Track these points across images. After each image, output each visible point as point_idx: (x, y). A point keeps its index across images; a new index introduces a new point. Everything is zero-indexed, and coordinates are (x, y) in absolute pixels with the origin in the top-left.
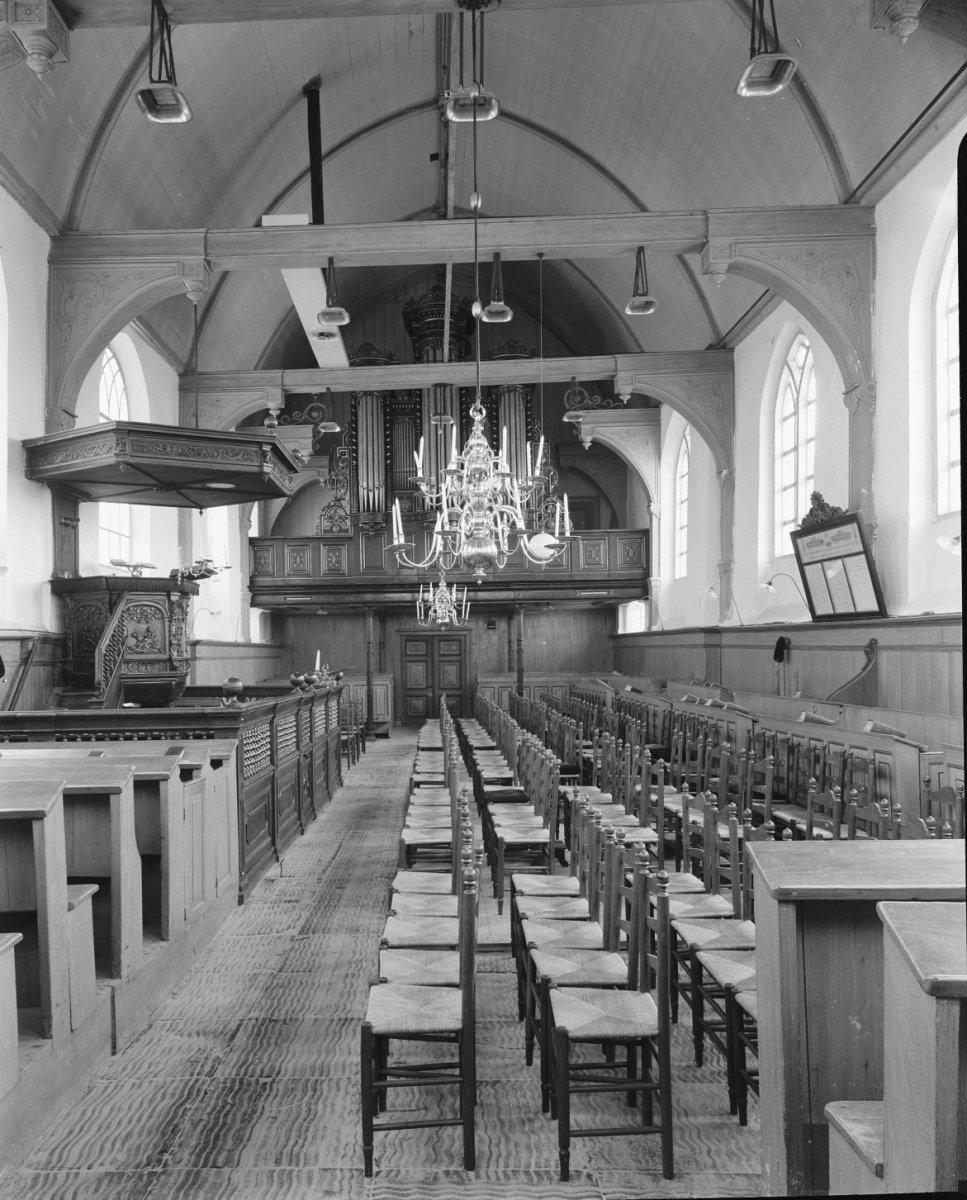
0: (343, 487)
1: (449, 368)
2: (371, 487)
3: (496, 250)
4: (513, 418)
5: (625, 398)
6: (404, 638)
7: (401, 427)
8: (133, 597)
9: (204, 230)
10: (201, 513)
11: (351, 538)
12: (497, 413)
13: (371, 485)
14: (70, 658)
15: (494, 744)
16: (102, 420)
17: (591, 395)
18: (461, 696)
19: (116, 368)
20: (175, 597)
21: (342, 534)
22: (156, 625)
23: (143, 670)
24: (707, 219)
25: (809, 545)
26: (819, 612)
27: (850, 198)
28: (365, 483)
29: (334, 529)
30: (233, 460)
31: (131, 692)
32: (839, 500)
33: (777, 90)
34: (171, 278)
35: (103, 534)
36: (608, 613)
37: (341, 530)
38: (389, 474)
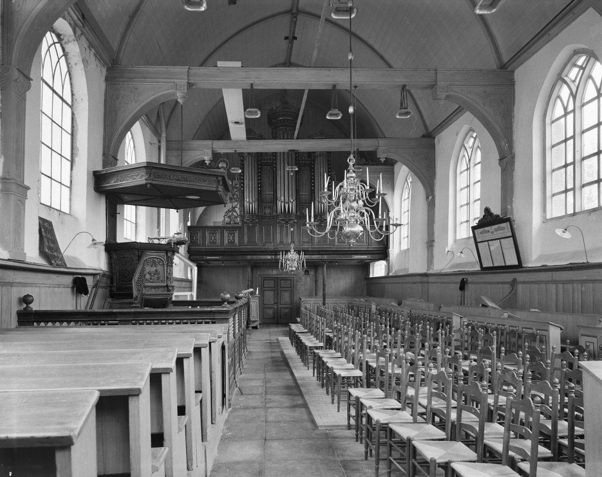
0: (236, 201)
1: (297, 142)
2: (251, 202)
3: (334, 83)
4: (322, 168)
5: (383, 160)
6: (263, 279)
8: (150, 253)
12: (314, 166)
13: (251, 200)
14: (115, 284)
15: (307, 330)
16: (126, 164)
18: (291, 308)
19: (61, 53)
20: (169, 254)
21: (236, 225)
22: (159, 268)
23: (153, 291)
24: (436, 73)
25: (481, 233)
26: (484, 266)
27: (503, 67)
28: (248, 200)
30: (203, 184)
31: (148, 303)
32: (496, 211)
33: (493, 11)
34: (171, 91)
36: (365, 267)
37: (235, 223)
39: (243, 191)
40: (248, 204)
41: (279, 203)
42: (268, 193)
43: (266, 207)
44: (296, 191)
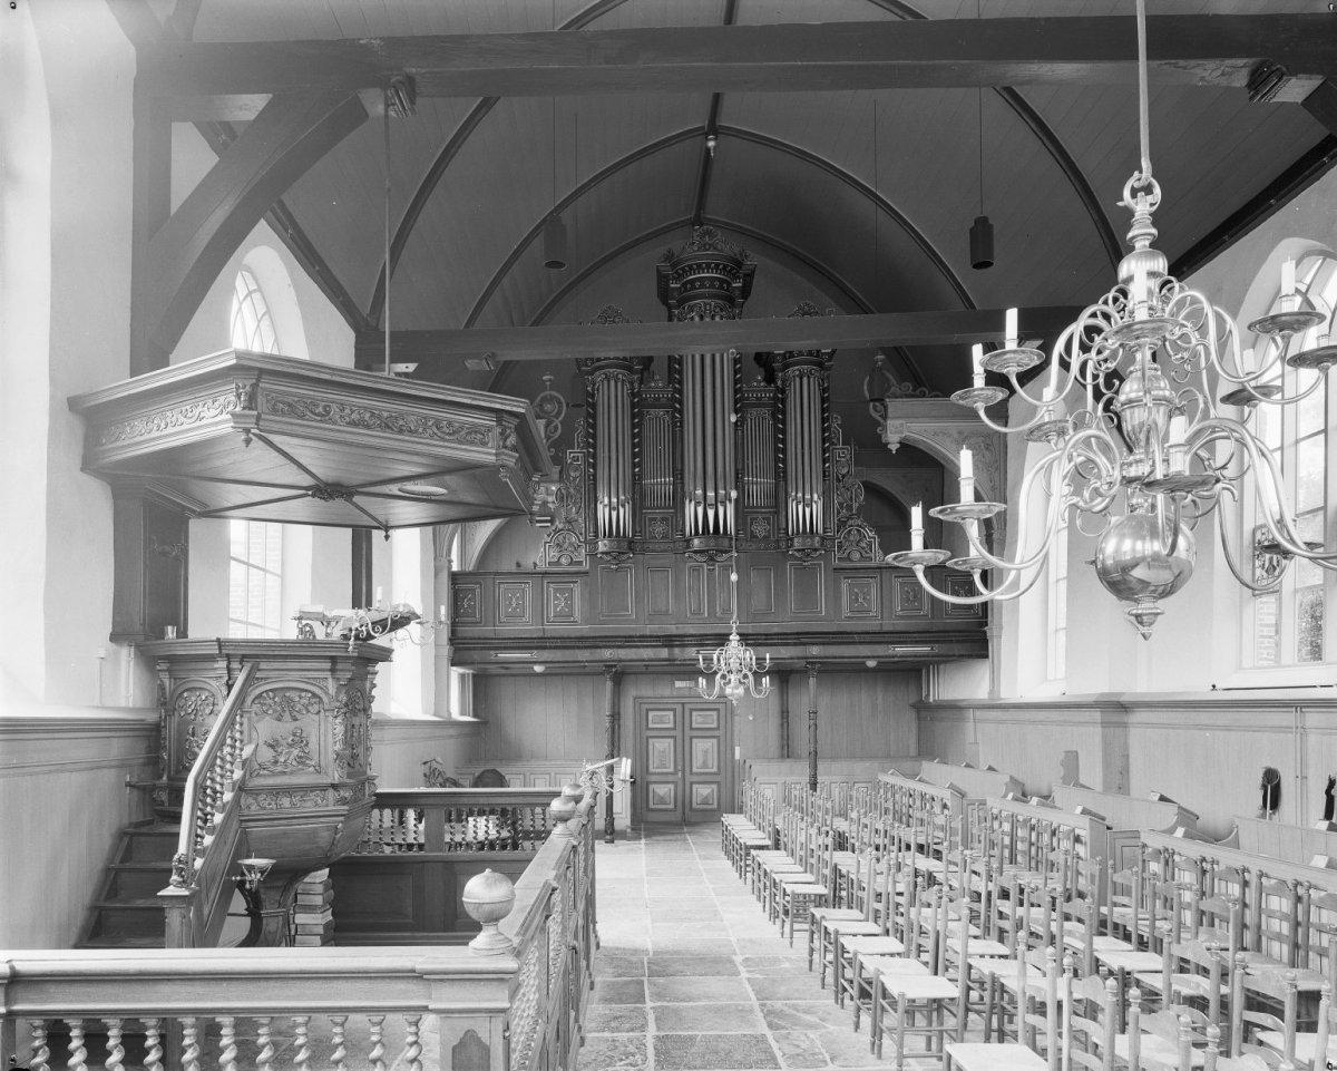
9: (234, 386)
10: (387, 537)
11: (586, 573)
29: (563, 560)
35: (236, 572)
39: (595, 475)
40: (607, 510)
41: (689, 509)
42: (660, 483)
43: (655, 519)
44: (737, 474)
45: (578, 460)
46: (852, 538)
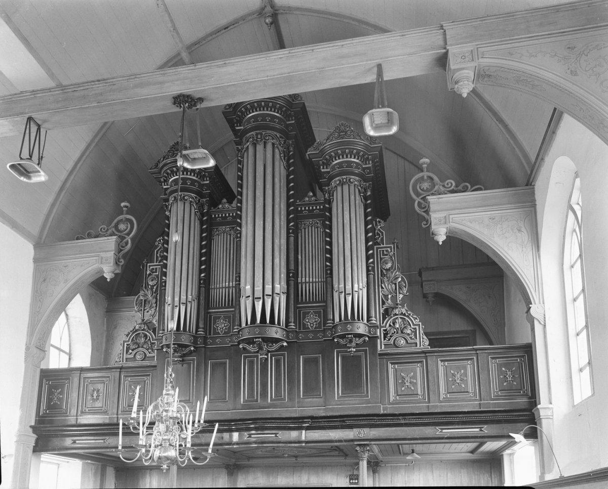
7: (221, 238)
17: (442, 180)
38: (292, 283)
45: (156, 272)
46: (397, 326)
